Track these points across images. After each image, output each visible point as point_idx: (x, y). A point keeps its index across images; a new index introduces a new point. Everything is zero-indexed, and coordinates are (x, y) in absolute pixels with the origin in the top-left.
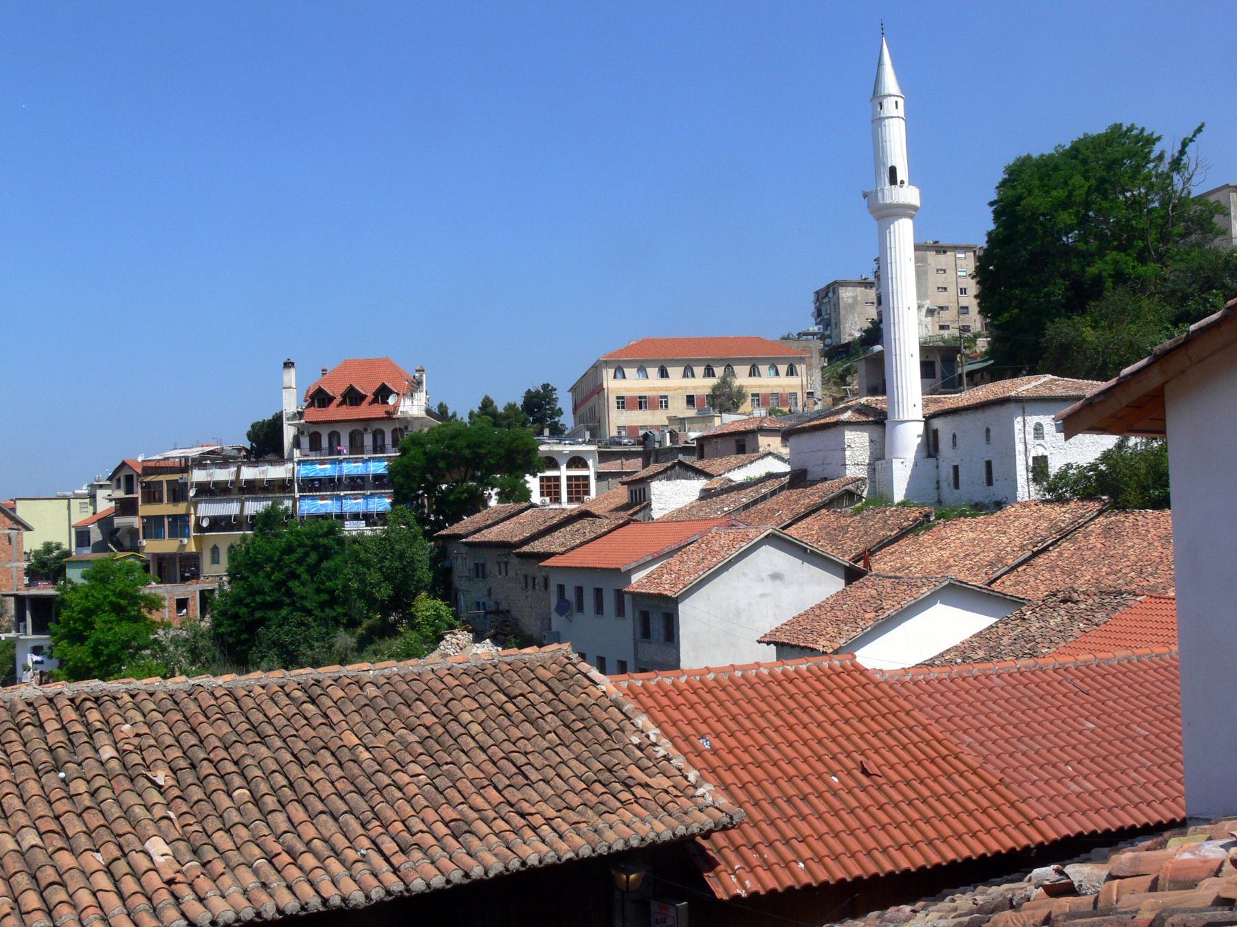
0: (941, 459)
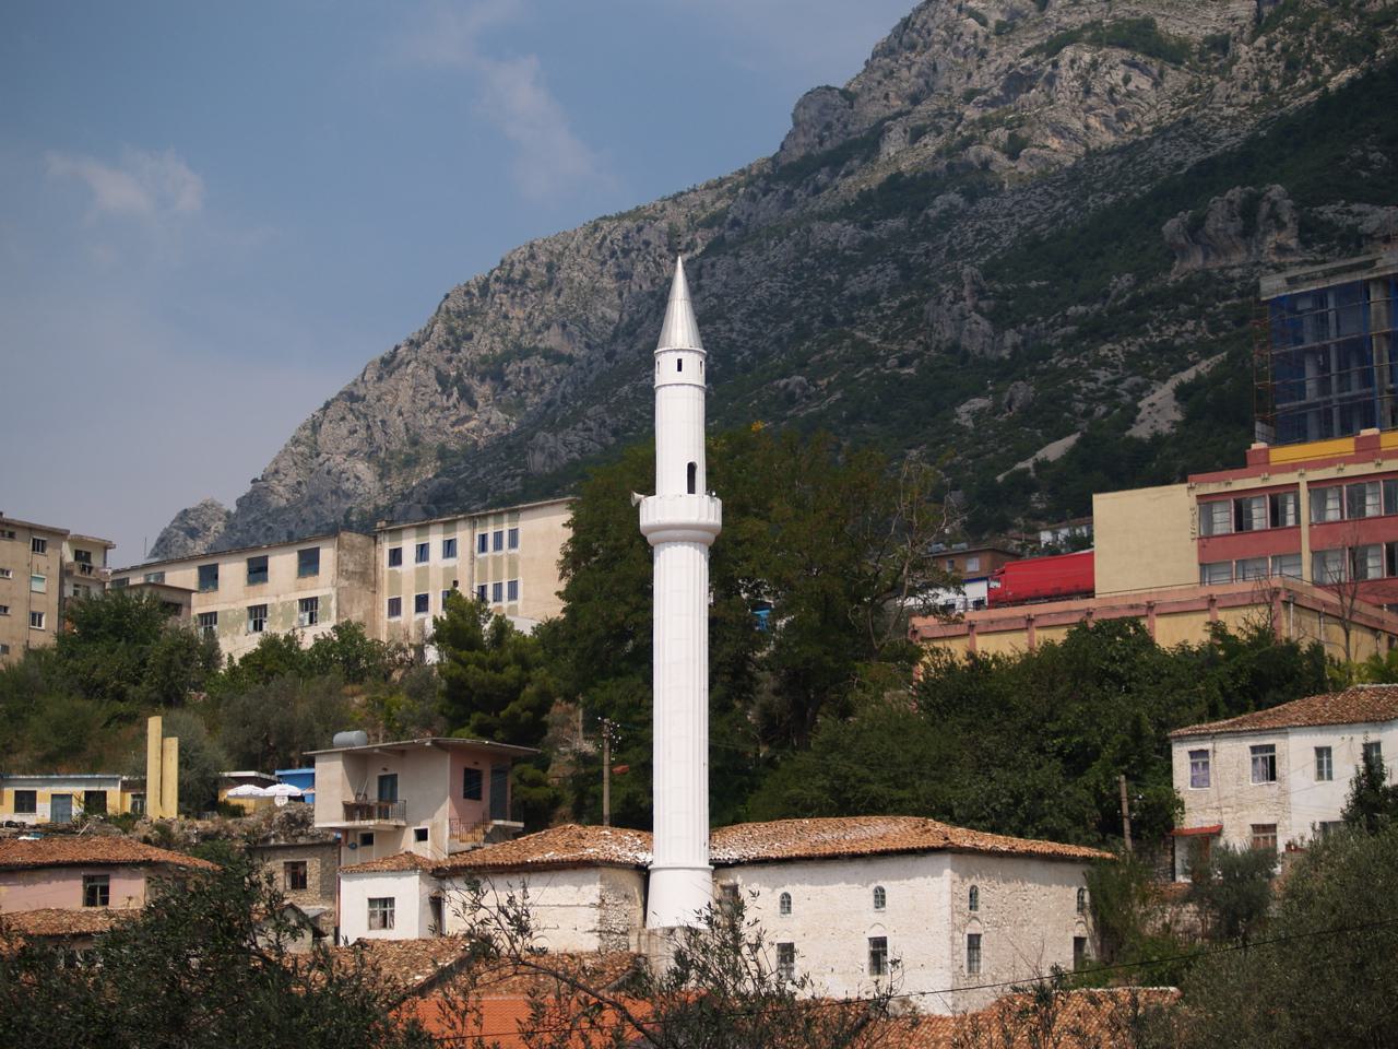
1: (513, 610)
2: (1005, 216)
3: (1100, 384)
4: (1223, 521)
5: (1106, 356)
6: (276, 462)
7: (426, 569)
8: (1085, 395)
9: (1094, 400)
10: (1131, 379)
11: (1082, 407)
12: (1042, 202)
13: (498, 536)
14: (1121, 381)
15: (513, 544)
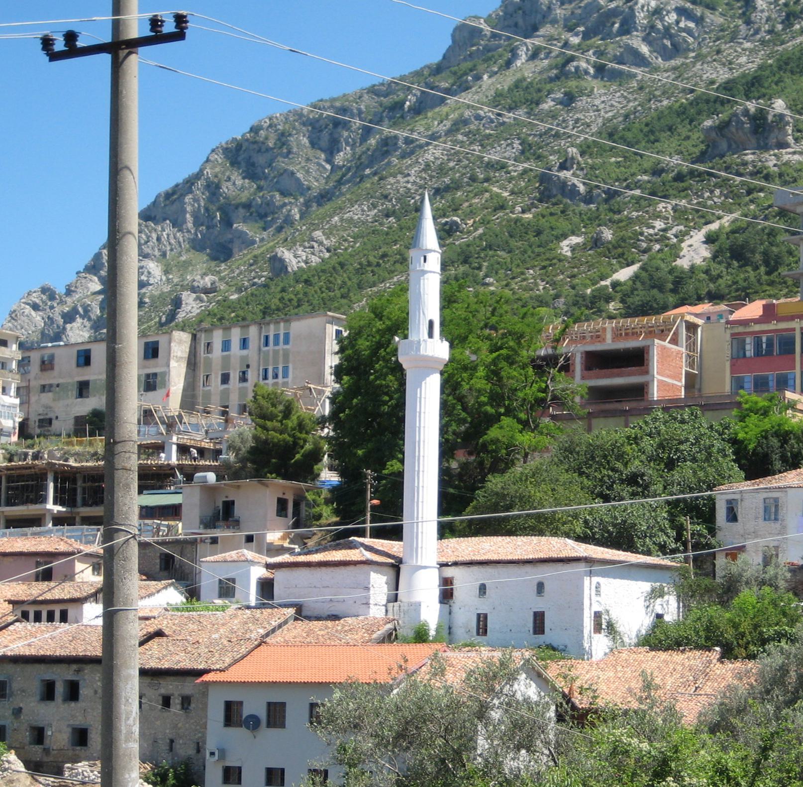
0: (455, 608)
1: (285, 384)
2: (594, 111)
5: (661, 212)
7: (228, 357)
8: (646, 237)
9: (651, 241)
11: (644, 245)
12: (619, 102)
13: (277, 336)
14: (671, 228)
15: (287, 341)
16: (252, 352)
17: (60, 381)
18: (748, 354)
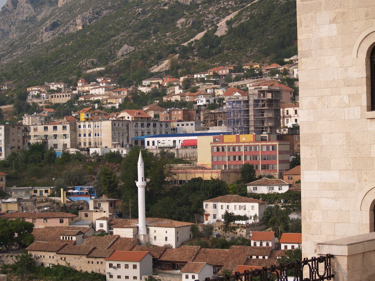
3: (209, 19)
4: (215, 149)
6: (7, 3)
7: (85, 129)
10: (217, 17)
15: (101, 126)
16: (91, 129)
17: (40, 134)
18: (215, 151)
